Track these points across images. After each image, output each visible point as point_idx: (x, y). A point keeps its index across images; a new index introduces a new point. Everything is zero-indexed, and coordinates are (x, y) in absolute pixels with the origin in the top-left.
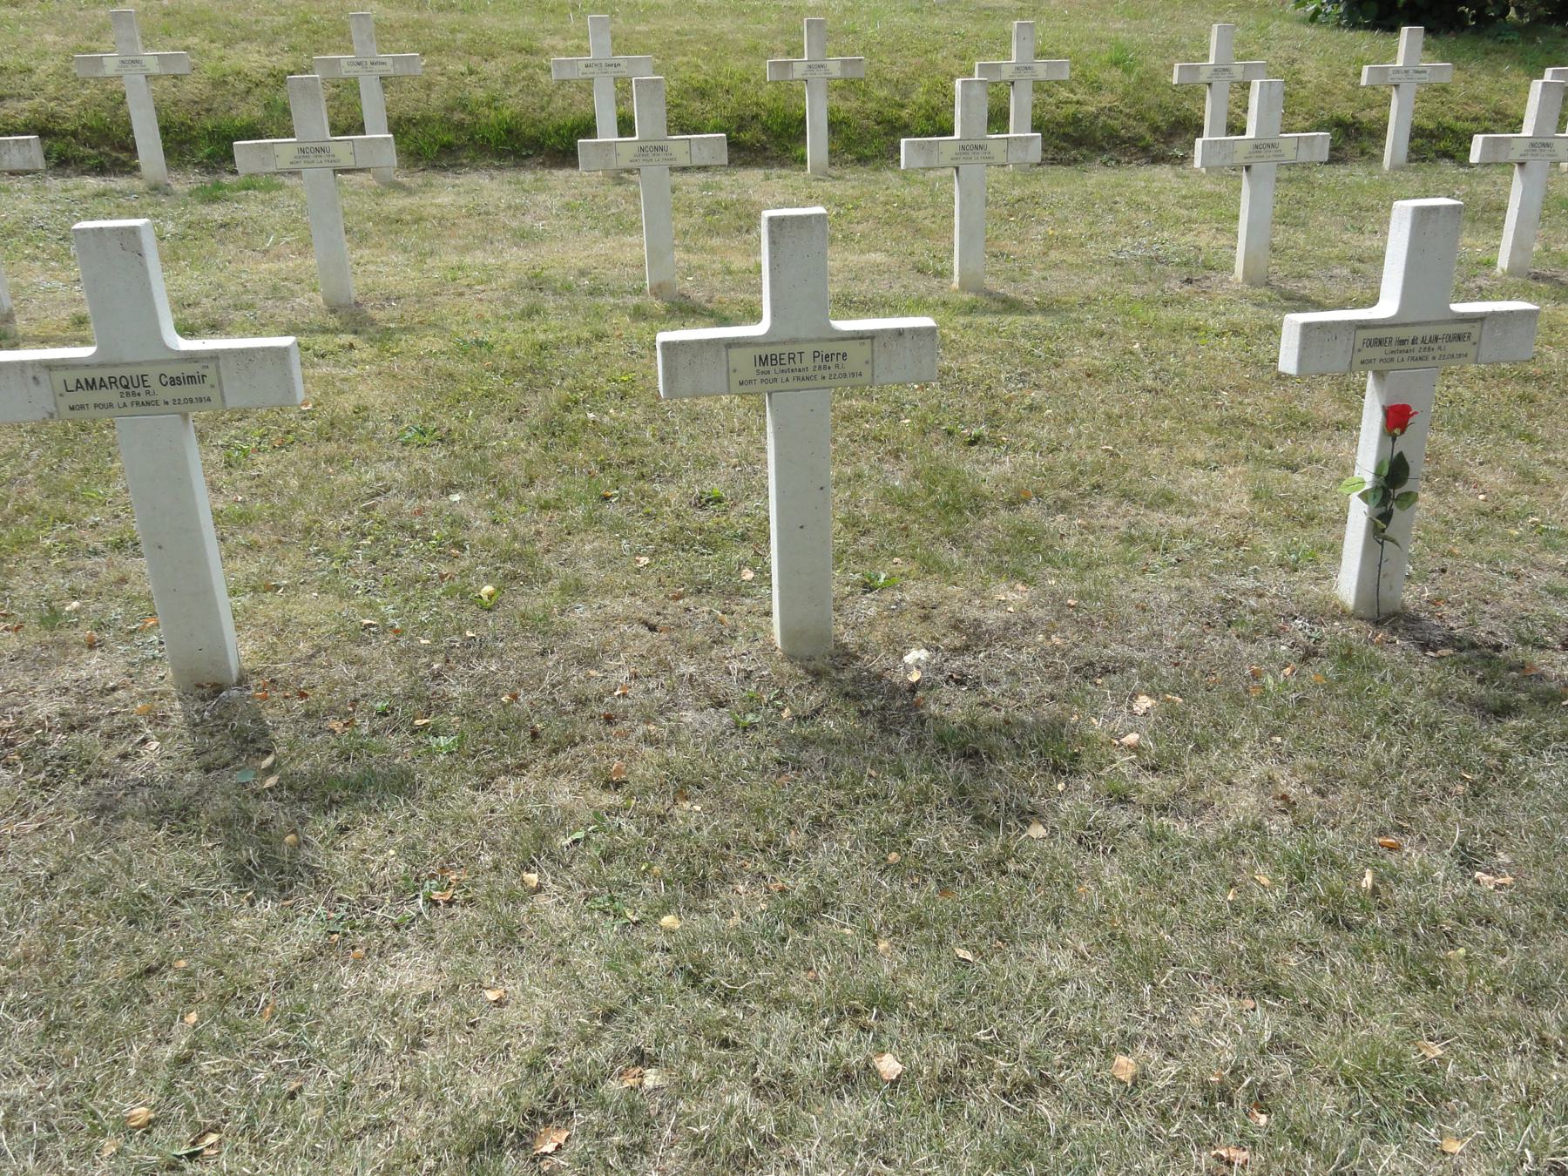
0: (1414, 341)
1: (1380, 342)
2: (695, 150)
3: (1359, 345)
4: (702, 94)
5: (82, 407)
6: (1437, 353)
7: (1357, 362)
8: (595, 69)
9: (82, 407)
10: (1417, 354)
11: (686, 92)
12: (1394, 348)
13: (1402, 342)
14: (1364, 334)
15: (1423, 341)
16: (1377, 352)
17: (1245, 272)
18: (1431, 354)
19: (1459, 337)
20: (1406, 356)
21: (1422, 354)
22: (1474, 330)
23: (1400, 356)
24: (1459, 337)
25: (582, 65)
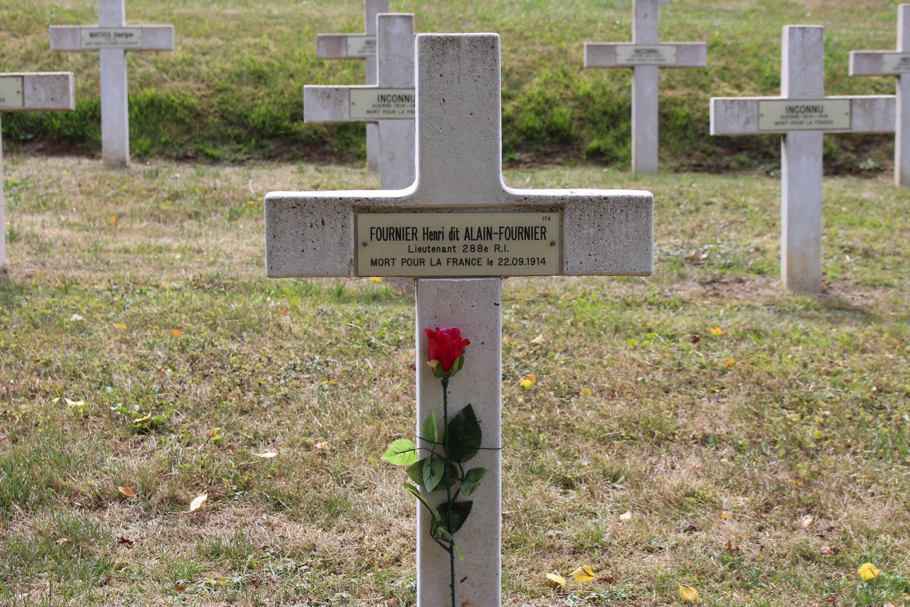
0: (453, 235)
1: (398, 234)
2: (28, 90)
3: (364, 235)
4: (259, 77)
5: (386, 262)
7: (365, 256)
8: (101, 39)
9: (386, 262)
10: (459, 255)
11: (239, 76)
12: (424, 244)
14: (368, 221)
15: (468, 235)
16: (396, 249)
17: (790, 275)
18: (484, 256)
19: (526, 233)
20: (443, 257)
21: (470, 255)
22: (552, 223)
23: (436, 256)
24: (526, 233)
25: (85, 34)
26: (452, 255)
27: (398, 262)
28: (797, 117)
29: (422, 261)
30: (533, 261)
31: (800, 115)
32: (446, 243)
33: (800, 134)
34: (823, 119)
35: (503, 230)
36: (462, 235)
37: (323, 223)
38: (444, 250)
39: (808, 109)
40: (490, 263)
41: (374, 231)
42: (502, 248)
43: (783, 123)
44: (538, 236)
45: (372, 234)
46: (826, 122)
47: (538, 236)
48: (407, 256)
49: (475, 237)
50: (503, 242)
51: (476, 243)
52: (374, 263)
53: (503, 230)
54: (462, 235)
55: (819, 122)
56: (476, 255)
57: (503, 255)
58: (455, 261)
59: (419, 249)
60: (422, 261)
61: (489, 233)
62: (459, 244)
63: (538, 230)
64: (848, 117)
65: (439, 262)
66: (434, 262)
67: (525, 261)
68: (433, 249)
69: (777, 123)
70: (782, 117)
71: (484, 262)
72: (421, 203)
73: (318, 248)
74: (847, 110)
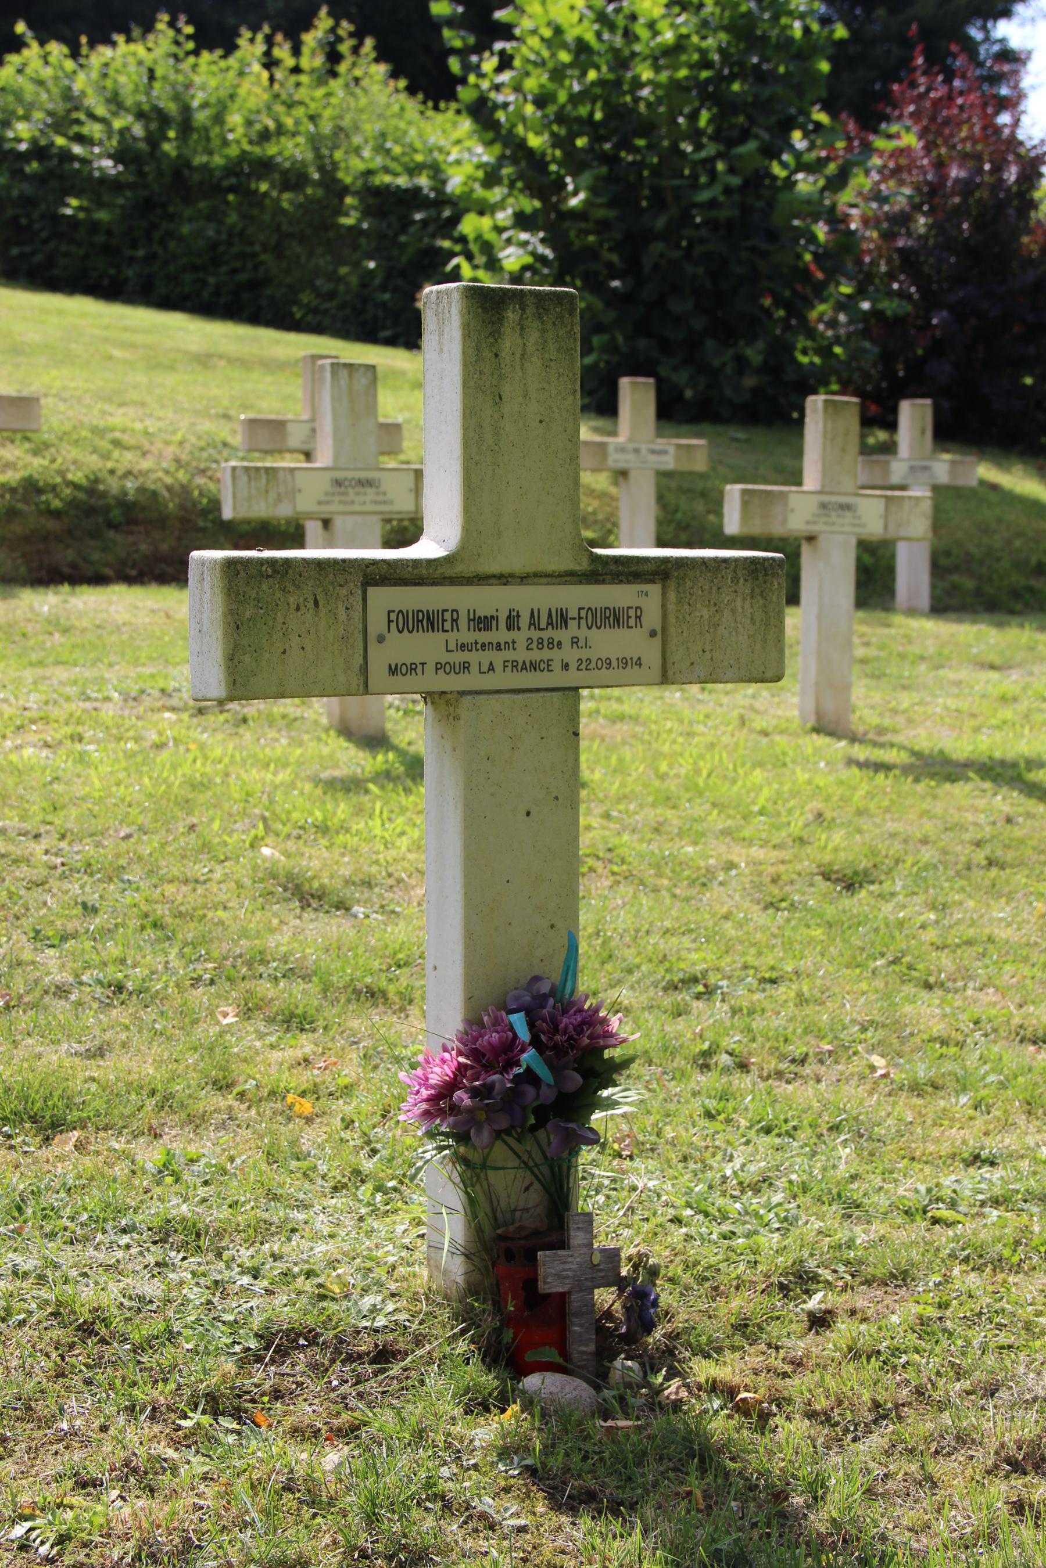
0: (513, 621)
1: (429, 621)
5: (412, 668)
6: (571, 655)
7: (380, 658)
9: (412, 668)
10: (521, 655)
12: (467, 636)
13: (484, 623)
16: (427, 646)
18: (556, 655)
19: (614, 618)
20: (498, 658)
21: (536, 655)
23: (486, 657)
24: (614, 618)
26: (509, 655)
27: (430, 668)
28: (346, 494)
29: (466, 667)
30: (624, 663)
31: (351, 491)
32: (501, 635)
33: (350, 520)
34: (381, 498)
35: (583, 613)
36: (524, 621)
37: (316, 603)
38: (499, 647)
39: (361, 483)
40: (566, 666)
41: (393, 616)
42: (582, 643)
43: (328, 503)
44: (632, 622)
45: (390, 621)
46: (384, 503)
47: (632, 622)
48: (444, 658)
49: (543, 625)
50: (583, 633)
51: (545, 635)
52: (393, 670)
53: (583, 613)
54: (524, 621)
55: (376, 502)
56: (545, 654)
57: (584, 654)
58: (515, 665)
59: (463, 646)
60: (466, 667)
61: (562, 619)
62: (521, 637)
63: (632, 613)
64: (412, 496)
65: (491, 668)
66: (485, 668)
67: (614, 663)
68: (483, 645)
69: (320, 503)
70: (326, 494)
71: (556, 666)
72: (460, 569)
73: (308, 648)
74: (412, 485)
